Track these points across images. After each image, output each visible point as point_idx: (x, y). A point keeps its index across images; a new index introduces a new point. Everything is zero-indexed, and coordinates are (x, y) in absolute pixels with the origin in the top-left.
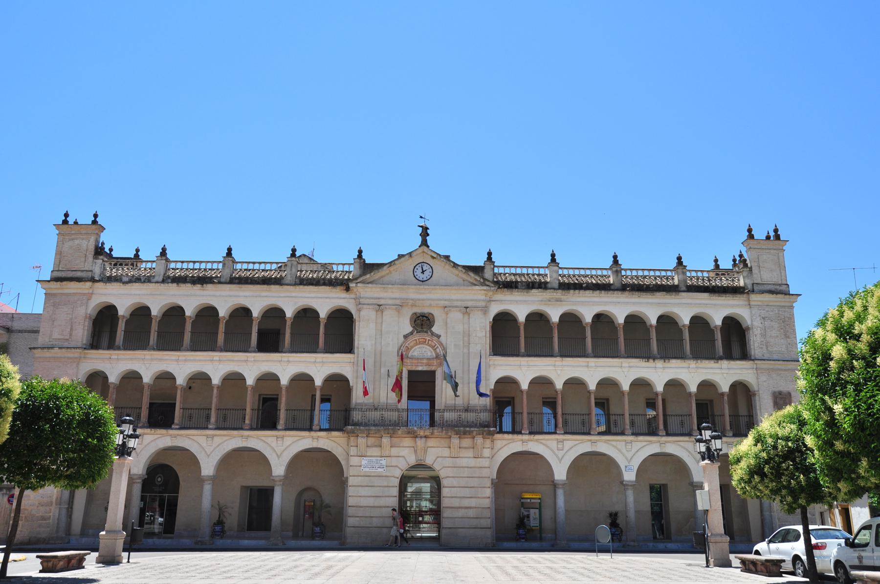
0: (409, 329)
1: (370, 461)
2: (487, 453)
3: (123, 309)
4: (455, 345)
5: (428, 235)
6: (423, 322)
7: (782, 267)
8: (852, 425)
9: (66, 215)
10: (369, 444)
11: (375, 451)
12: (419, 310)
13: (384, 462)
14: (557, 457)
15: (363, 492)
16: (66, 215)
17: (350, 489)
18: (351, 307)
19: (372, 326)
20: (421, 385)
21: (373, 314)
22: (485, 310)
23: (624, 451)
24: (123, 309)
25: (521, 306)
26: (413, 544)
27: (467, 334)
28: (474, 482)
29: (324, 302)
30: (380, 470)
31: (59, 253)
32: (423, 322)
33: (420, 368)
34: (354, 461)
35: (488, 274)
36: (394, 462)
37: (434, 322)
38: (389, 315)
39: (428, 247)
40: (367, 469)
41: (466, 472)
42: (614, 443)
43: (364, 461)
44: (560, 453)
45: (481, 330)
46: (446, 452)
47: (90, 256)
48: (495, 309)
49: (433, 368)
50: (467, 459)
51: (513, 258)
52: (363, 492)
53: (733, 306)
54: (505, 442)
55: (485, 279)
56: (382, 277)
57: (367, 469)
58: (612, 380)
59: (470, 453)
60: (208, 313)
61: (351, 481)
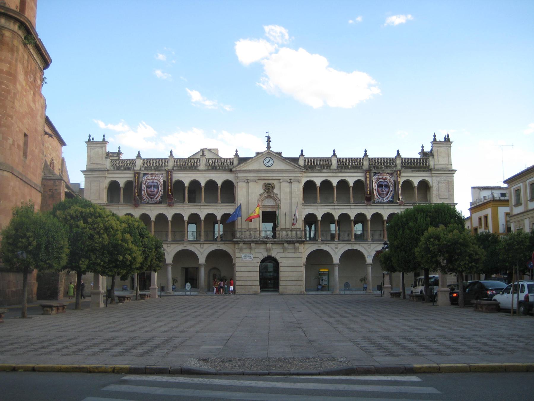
0: (262, 191)
3: (318, 182)
5: (280, 154)
7: (449, 155)
8: (482, 234)
9: (90, 136)
12: (267, 182)
14: (335, 251)
15: (243, 269)
16: (90, 136)
17: (237, 268)
21: (244, 184)
22: (299, 182)
23: (367, 248)
24: (318, 182)
25: (318, 179)
29: (219, 178)
31: (89, 157)
33: (268, 210)
34: (238, 255)
35: (301, 163)
36: (257, 255)
41: (291, 260)
42: (362, 245)
43: (243, 255)
44: (336, 250)
45: (298, 189)
46: (281, 251)
47: (104, 159)
48: (304, 180)
50: (291, 254)
51: (314, 152)
52: (243, 269)
53: (424, 177)
55: (299, 166)
58: (414, 240)
59: (293, 251)
60: (195, 184)
61: (237, 265)
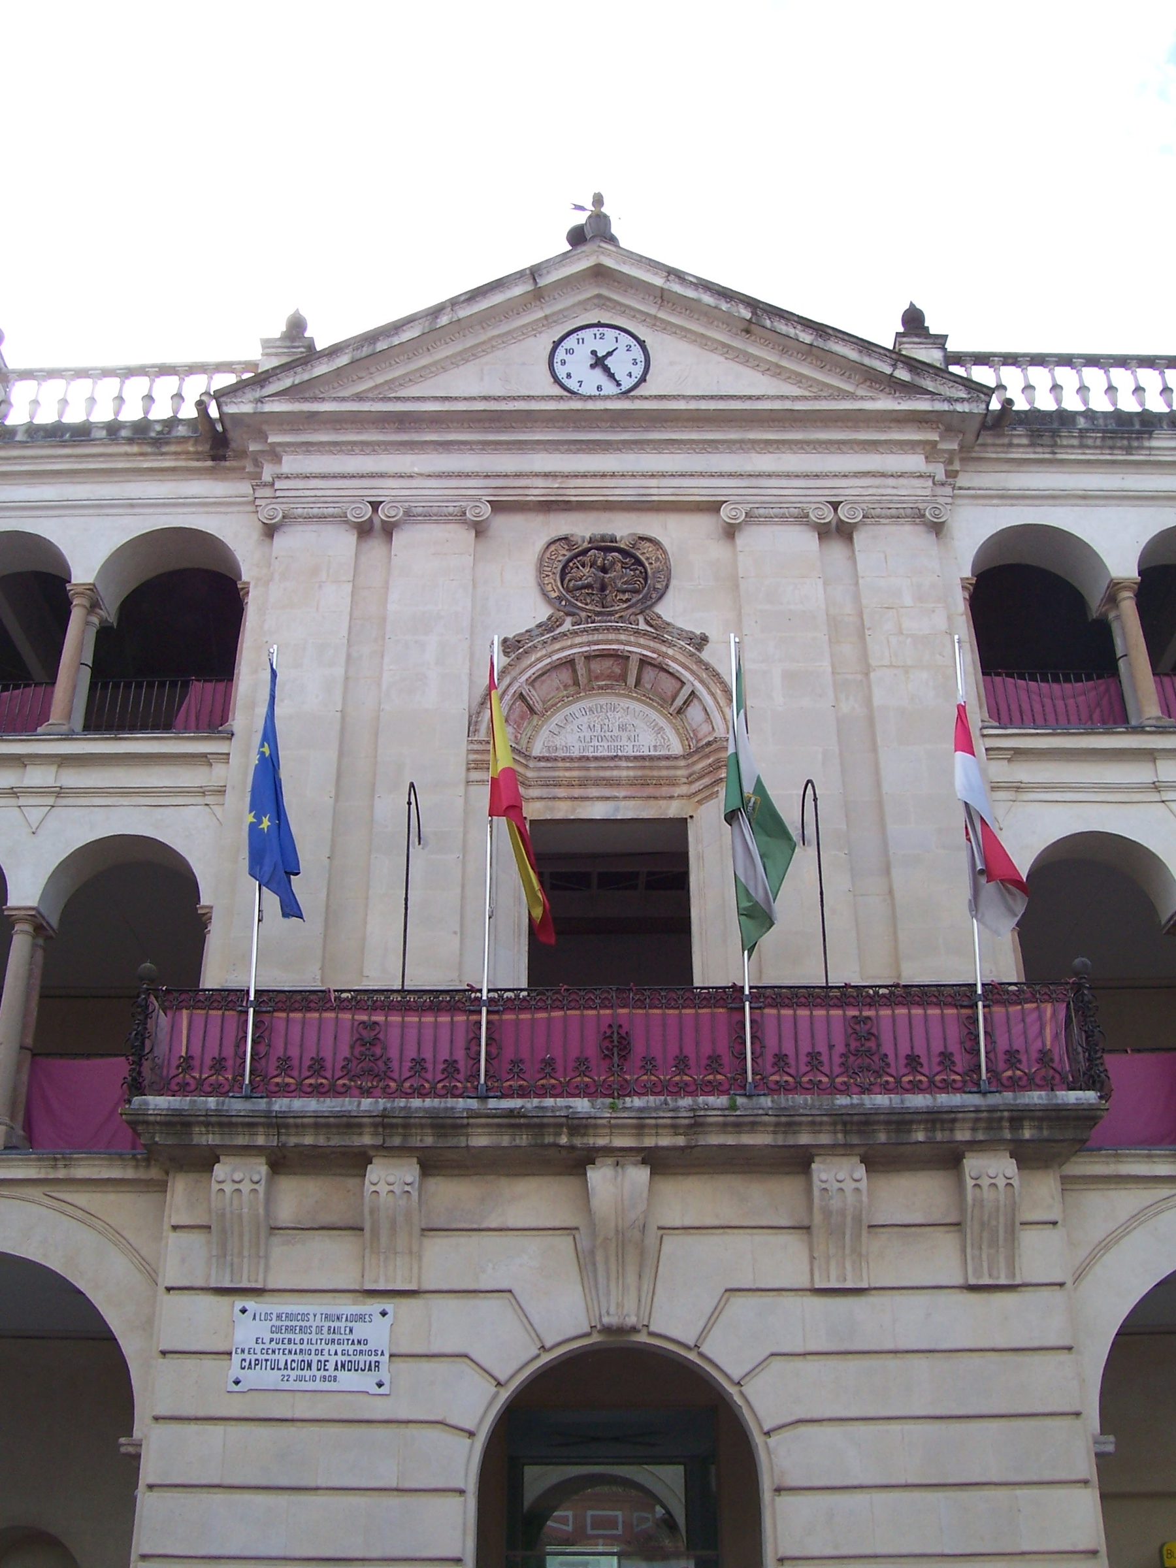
0: (529, 611)
1: (288, 1325)
2: (1040, 1254)
4: (790, 678)
6: (607, 579)
10: (286, 1212)
11: (330, 1261)
13: (377, 1329)
18: (235, 533)
19: (335, 598)
20: (608, 902)
26: (816, 326)
27: (852, 629)
28: (984, 1452)
30: (348, 1380)
32: (607, 579)
33: (598, 811)
36: (449, 1326)
37: (667, 574)
38: (427, 559)
39: (612, 240)
40: (270, 1378)
43: (250, 1327)
46: (786, 1260)
48: (975, 527)
49: (673, 810)
54: (1128, 1201)
56: (595, 1271)
57: (270, 1378)
59: (941, 1260)
